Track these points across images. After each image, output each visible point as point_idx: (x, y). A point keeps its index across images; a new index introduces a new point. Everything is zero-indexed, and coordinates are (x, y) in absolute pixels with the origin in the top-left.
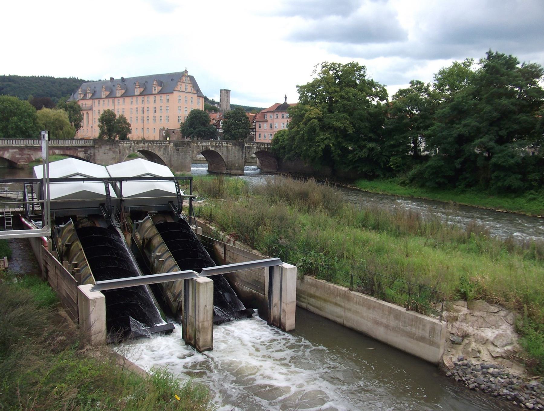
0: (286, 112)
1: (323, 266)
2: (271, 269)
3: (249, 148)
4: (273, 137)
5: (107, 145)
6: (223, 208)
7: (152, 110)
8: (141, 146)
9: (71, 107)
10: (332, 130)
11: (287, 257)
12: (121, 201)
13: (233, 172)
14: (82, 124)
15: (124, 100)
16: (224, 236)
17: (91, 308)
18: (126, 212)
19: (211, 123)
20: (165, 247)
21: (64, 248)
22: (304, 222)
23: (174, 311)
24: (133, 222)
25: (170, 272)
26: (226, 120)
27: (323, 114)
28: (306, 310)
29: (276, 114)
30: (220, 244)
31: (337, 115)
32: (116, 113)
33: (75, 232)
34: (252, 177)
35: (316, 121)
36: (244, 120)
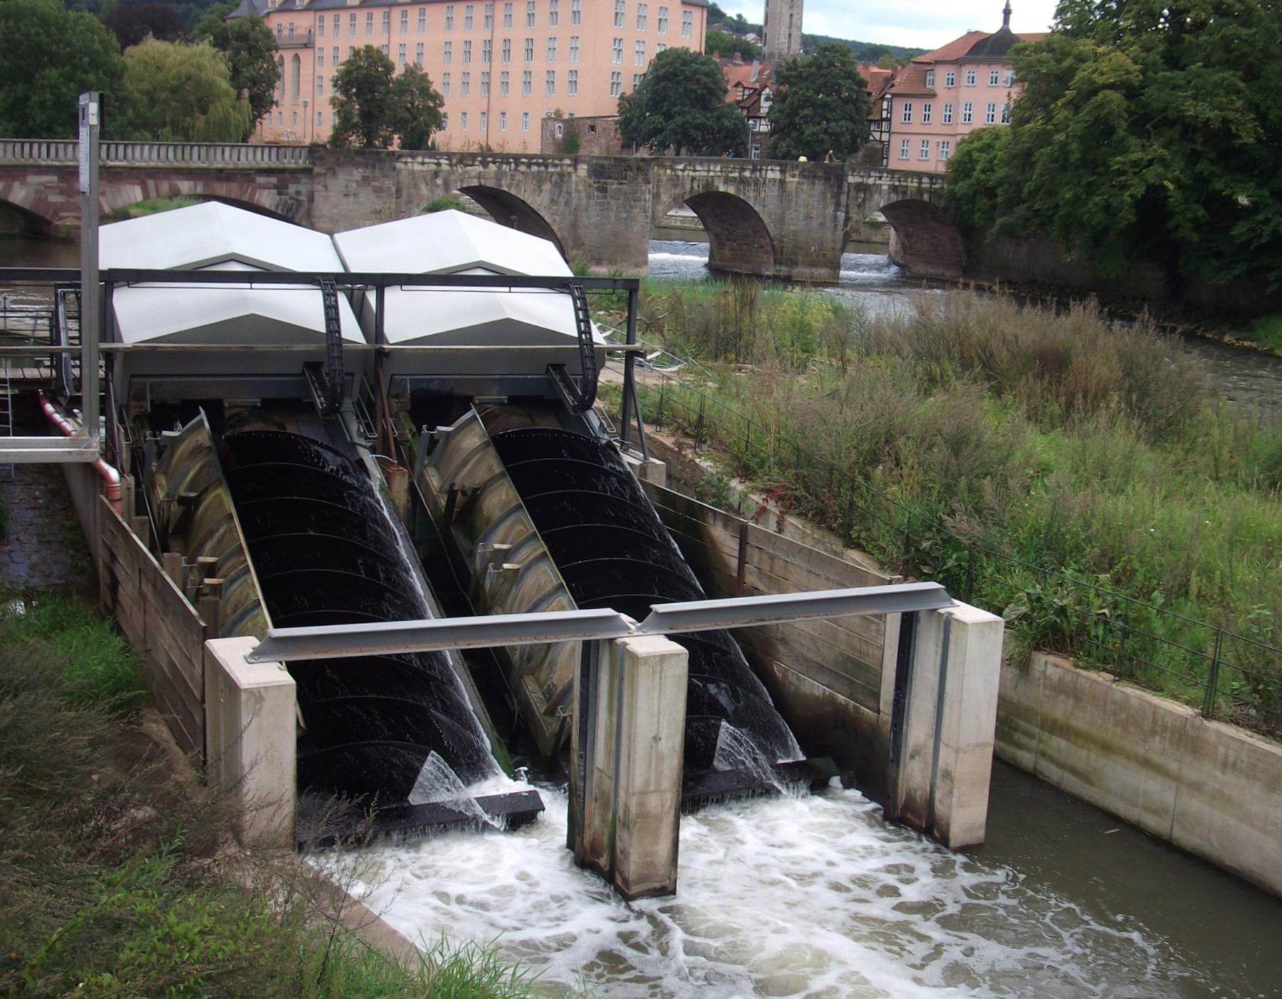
0: (1004, 64)
1: (1106, 623)
2: (909, 624)
3: (861, 188)
4: (951, 152)
5: (357, 166)
6: (746, 393)
7: (518, 50)
8: (474, 174)
9: (242, 37)
10: (1175, 132)
11: (971, 580)
12: (378, 354)
13: (801, 271)
14: (276, 95)
15: (422, 13)
16: (744, 496)
17: (245, 719)
18: (397, 396)
19: (729, 99)
20: (525, 524)
21: (175, 507)
22: (1045, 457)
23: (547, 749)
24: (419, 430)
25: (538, 610)
26: (784, 88)
27: (1143, 72)
28: (1033, 777)
29: (966, 71)
30: (727, 522)
31: (1198, 76)
32: (394, 57)
33: (213, 458)
34: (869, 291)
35: (1115, 96)
36: (850, 90)
